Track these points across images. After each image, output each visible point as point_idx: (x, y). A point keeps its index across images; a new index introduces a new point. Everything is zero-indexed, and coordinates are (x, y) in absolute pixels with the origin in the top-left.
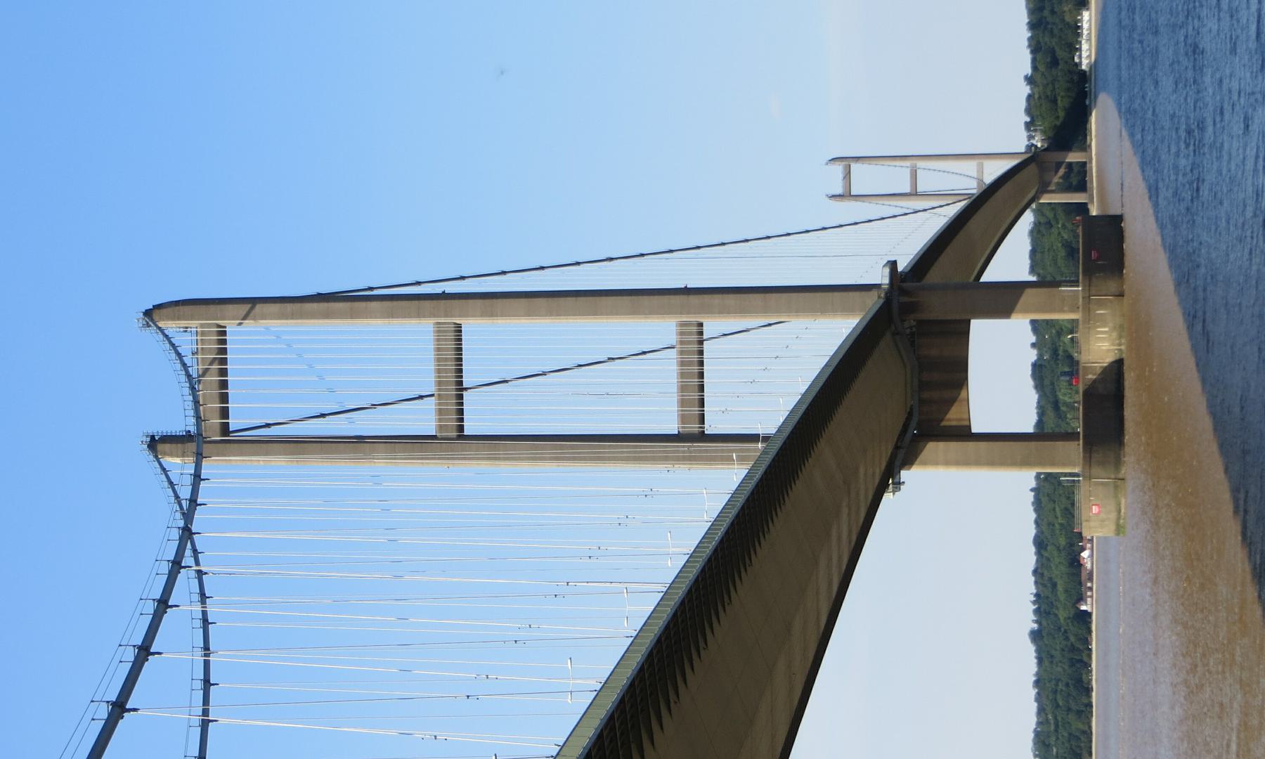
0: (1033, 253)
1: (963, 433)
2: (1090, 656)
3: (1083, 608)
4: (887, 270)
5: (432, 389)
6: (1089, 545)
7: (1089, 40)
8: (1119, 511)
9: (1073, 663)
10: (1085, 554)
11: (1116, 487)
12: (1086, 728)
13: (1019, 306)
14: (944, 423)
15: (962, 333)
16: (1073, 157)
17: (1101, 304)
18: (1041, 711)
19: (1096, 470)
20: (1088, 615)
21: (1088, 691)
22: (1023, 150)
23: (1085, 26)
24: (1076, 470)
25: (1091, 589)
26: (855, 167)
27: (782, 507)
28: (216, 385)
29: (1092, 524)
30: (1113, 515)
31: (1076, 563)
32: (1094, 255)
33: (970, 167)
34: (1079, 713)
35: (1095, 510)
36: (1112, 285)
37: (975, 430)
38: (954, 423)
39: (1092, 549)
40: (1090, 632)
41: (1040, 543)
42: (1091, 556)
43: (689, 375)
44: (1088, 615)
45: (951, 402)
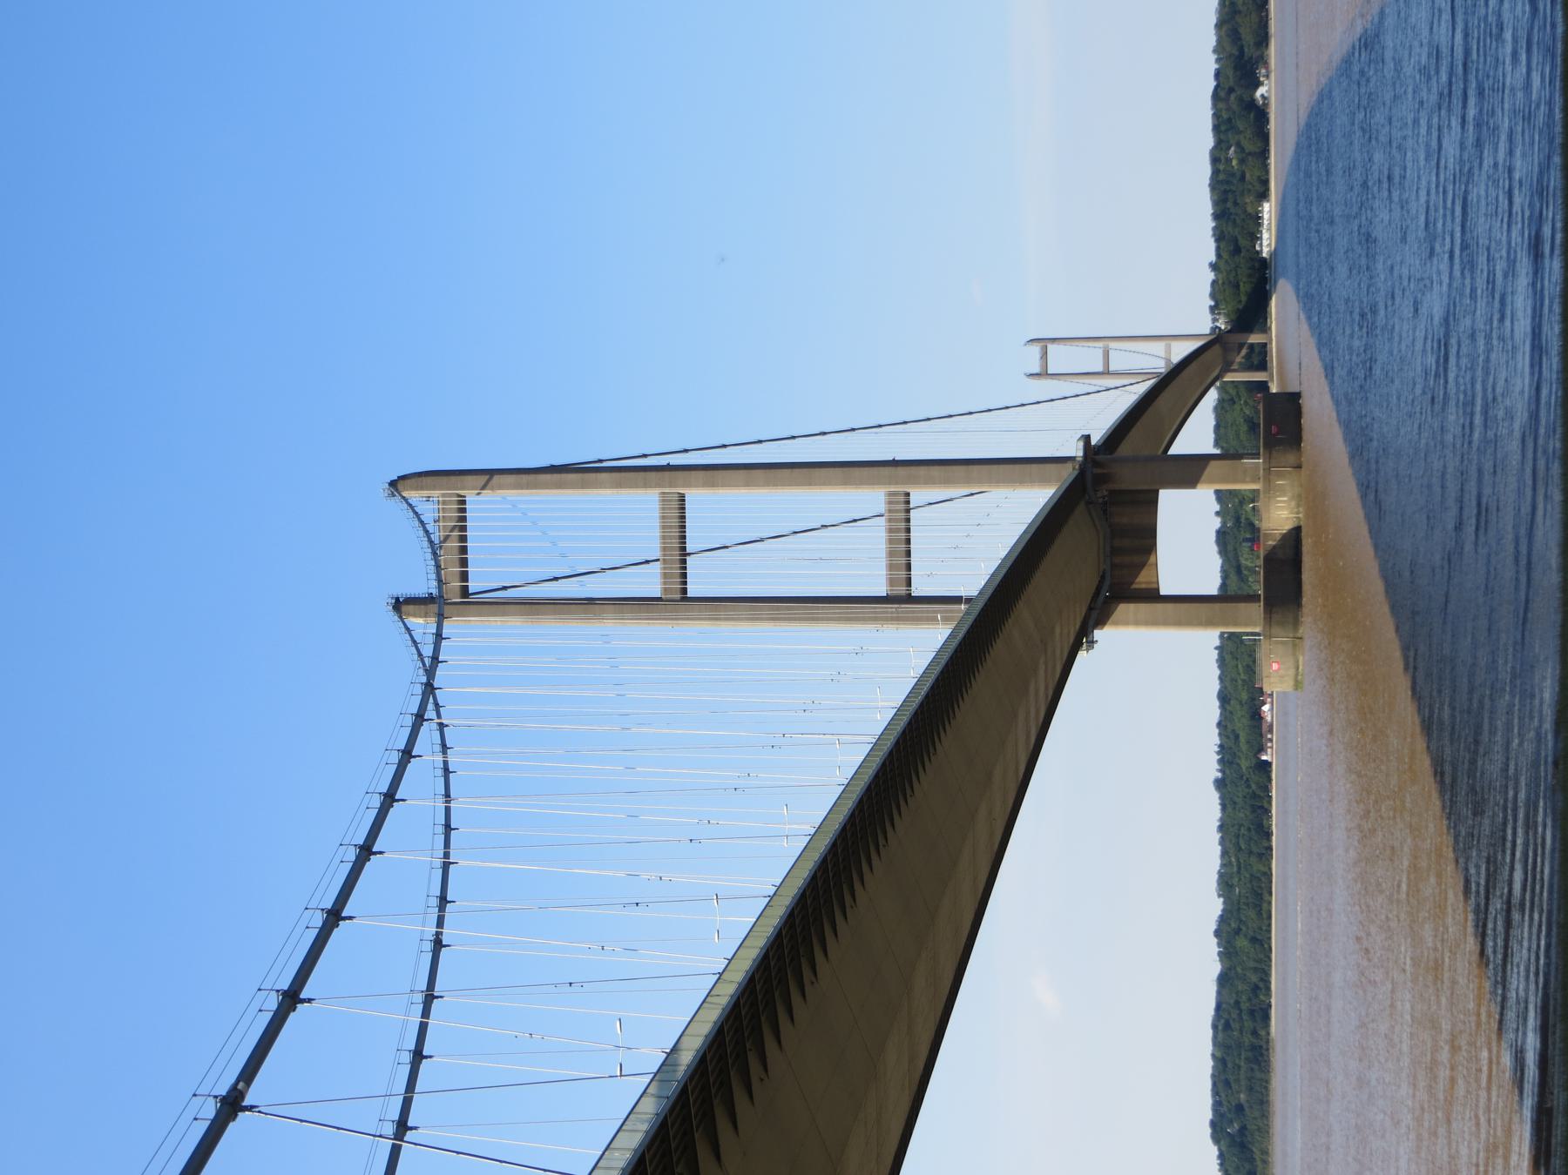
0: (1217, 428)
2: (1270, 803)
3: (1264, 758)
4: (1081, 444)
5: (657, 554)
6: (1269, 700)
9: (1254, 809)
10: (1266, 708)
11: (1295, 646)
12: (1266, 870)
13: (1203, 478)
14: (1134, 586)
15: (1152, 503)
16: (1255, 338)
17: (1280, 476)
18: (1225, 854)
19: (1276, 630)
21: (1268, 835)
22: (1208, 332)
24: (1257, 630)
25: (1271, 740)
26: (1051, 348)
27: (932, 758)
30: (1292, 672)
31: (1257, 716)
33: (1158, 348)
34: (1260, 855)
35: (1275, 666)
36: (1291, 458)
37: (1163, 592)
38: (1144, 586)
40: (1270, 780)
41: (1224, 698)
42: (1271, 709)
43: (898, 541)
44: (1268, 764)
45: (1142, 565)
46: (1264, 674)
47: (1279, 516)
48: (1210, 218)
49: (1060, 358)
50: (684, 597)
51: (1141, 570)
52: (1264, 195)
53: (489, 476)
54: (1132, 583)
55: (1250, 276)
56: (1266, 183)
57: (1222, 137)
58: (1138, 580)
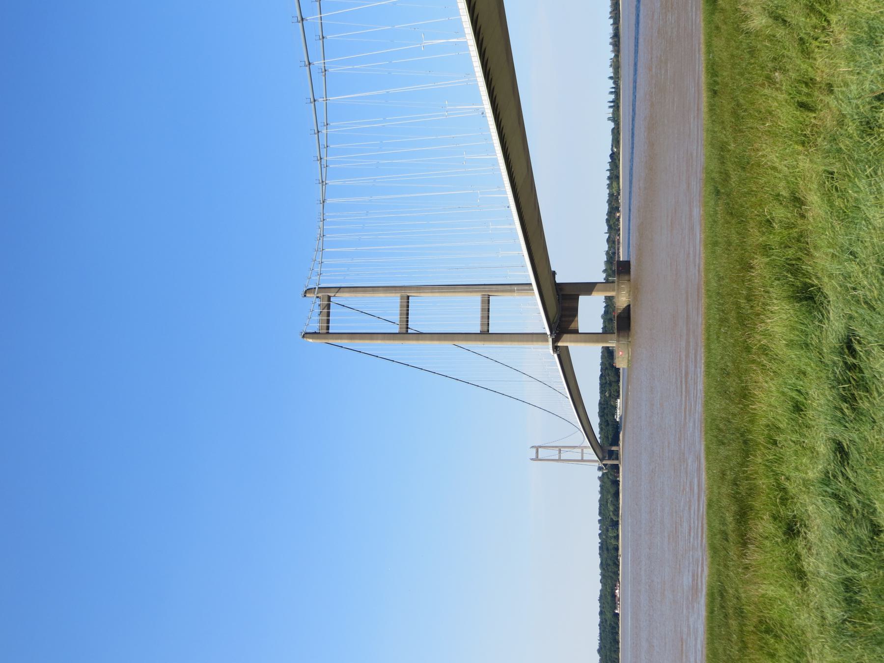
1: (576, 332)
2: (619, 629)
3: (616, 611)
6: (618, 588)
7: (620, 409)
8: (629, 354)
9: (613, 633)
11: (628, 344)
12: (617, 657)
14: (569, 329)
16: (614, 448)
17: (623, 284)
18: (602, 638)
19: (621, 339)
20: (618, 614)
21: (618, 642)
23: (619, 404)
24: (614, 346)
25: (619, 604)
28: (405, 328)
29: (620, 359)
30: (627, 356)
32: (620, 269)
34: (615, 651)
35: (621, 353)
36: (626, 277)
38: (573, 328)
39: (619, 589)
40: (619, 620)
42: (619, 592)
44: (618, 614)
45: (572, 321)
46: (617, 357)
47: (622, 301)
48: (598, 493)
49: (543, 453)
50: (407, 333)
51: (571, 323)
52: (618, 397)
53: (339, 289)
54: (569, 327)
55: (613, 430)
56: (619, 392)
57: (603, 389)
58: (571, 326)
